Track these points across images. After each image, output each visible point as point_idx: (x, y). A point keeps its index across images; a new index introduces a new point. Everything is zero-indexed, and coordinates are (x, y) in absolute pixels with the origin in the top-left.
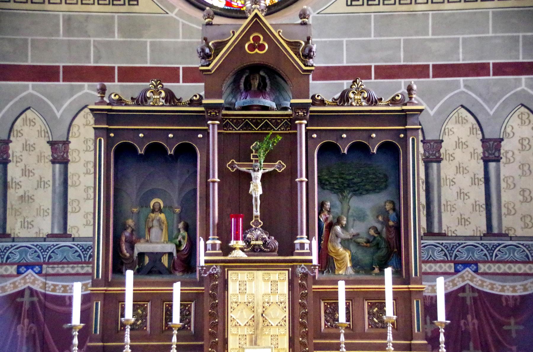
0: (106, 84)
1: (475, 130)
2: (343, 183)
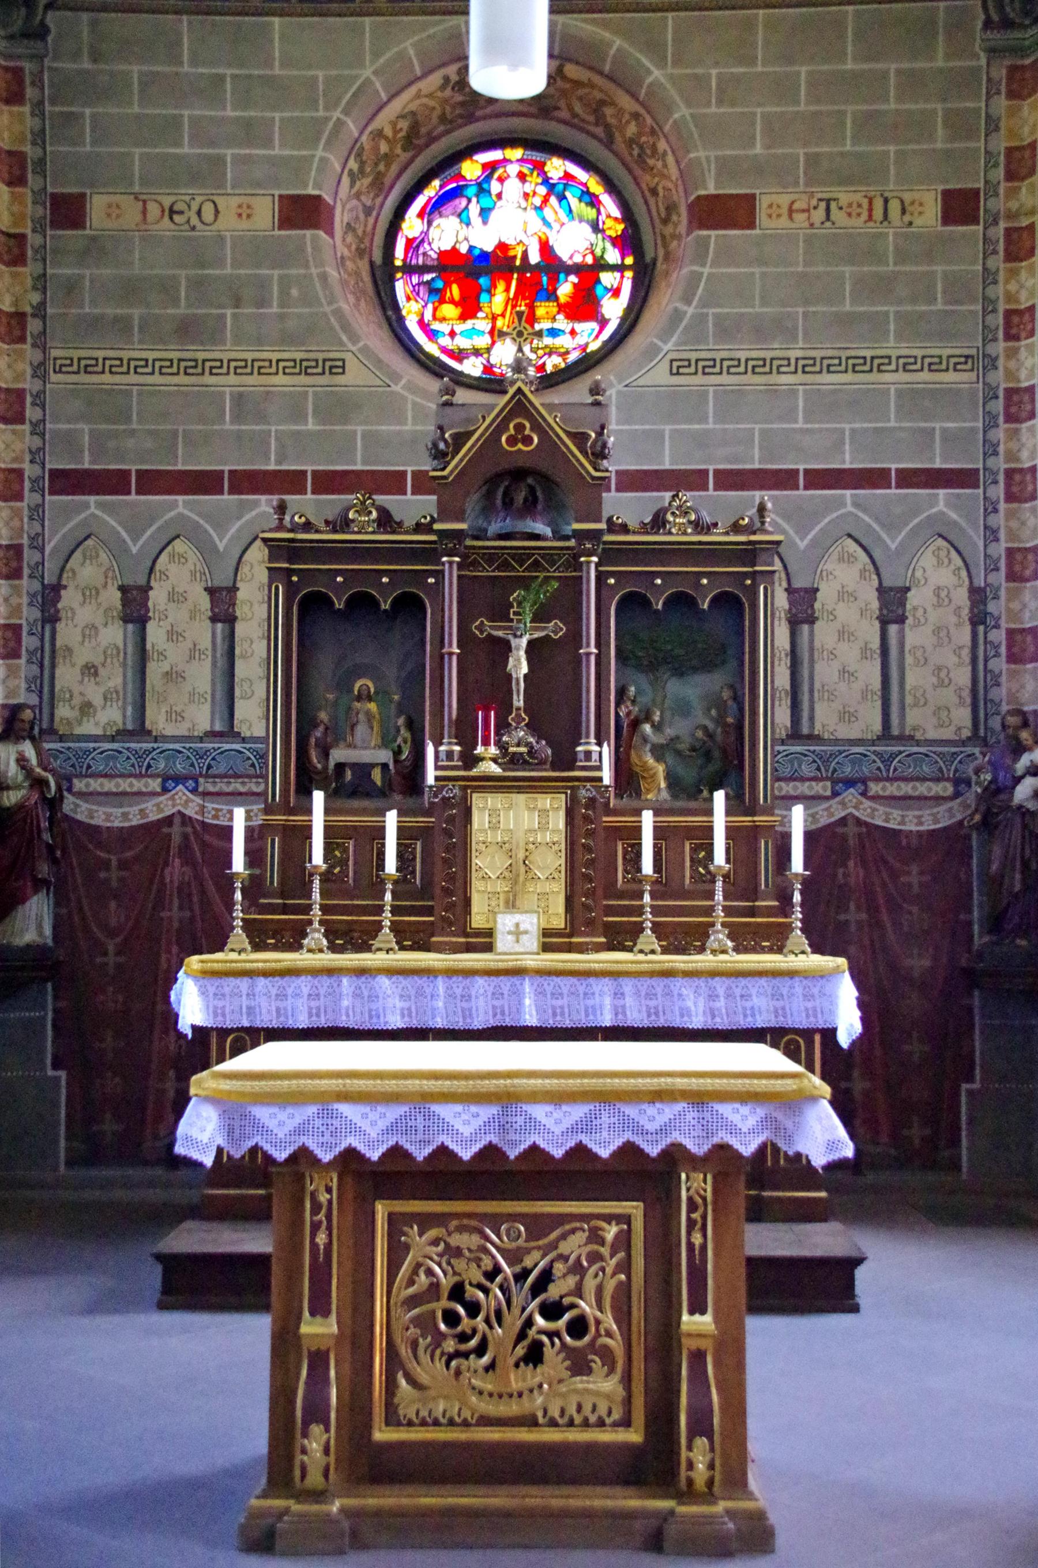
0: (286, 497)
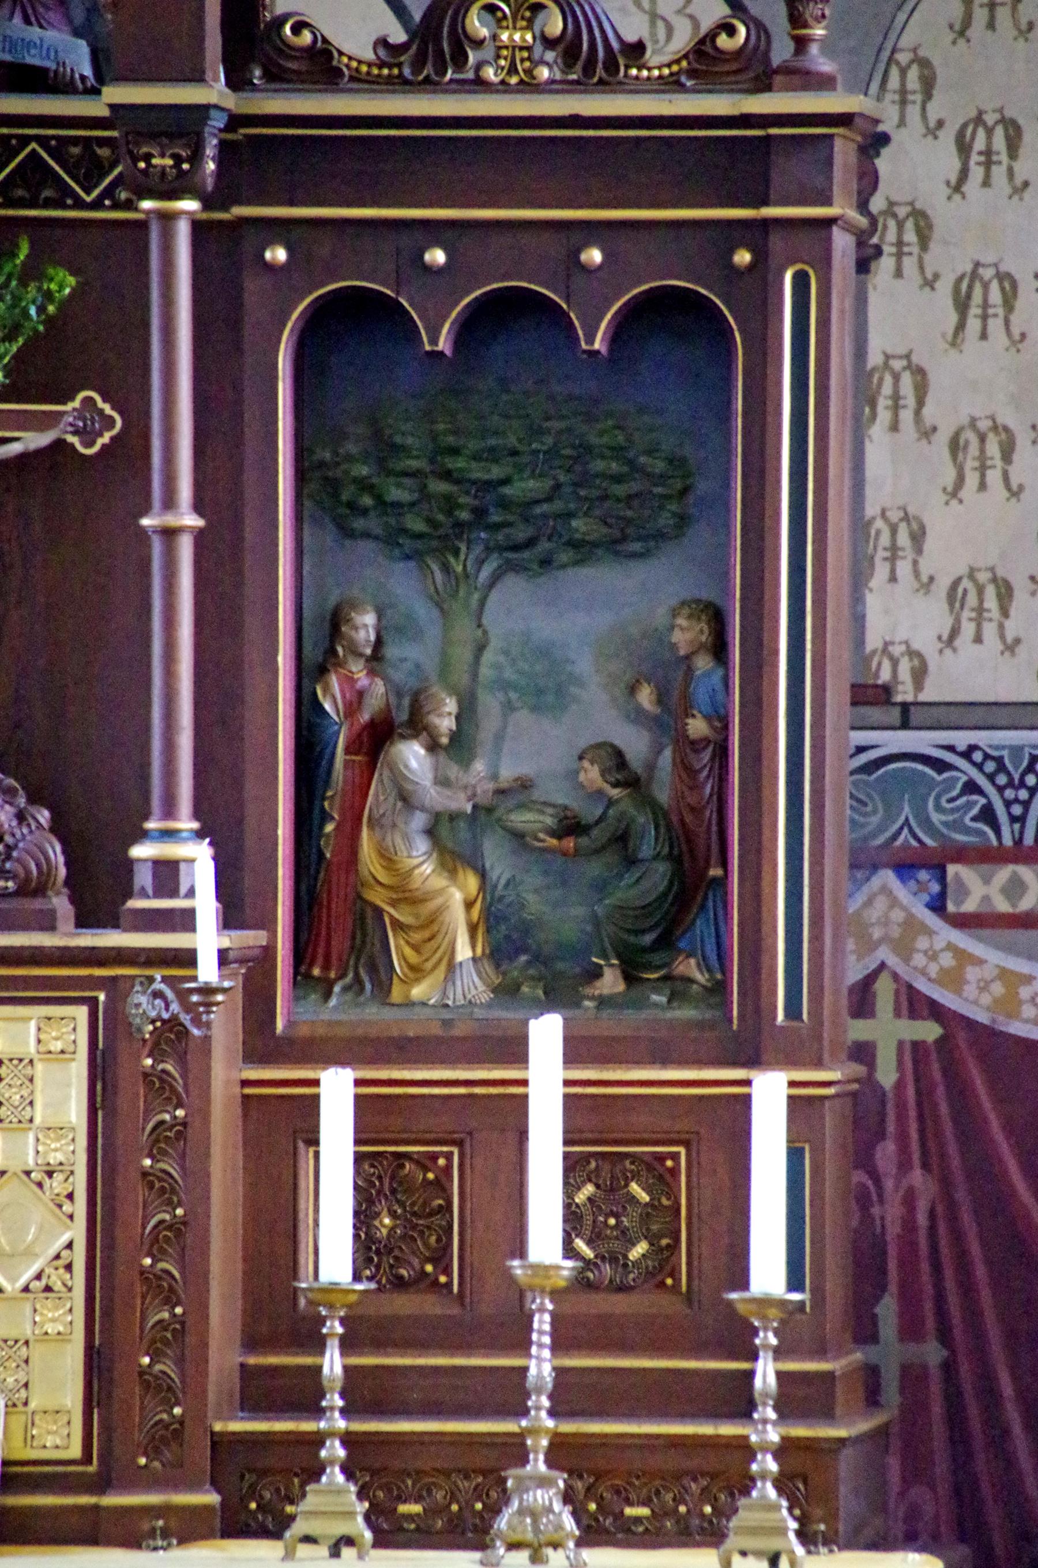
2: (450, 504)
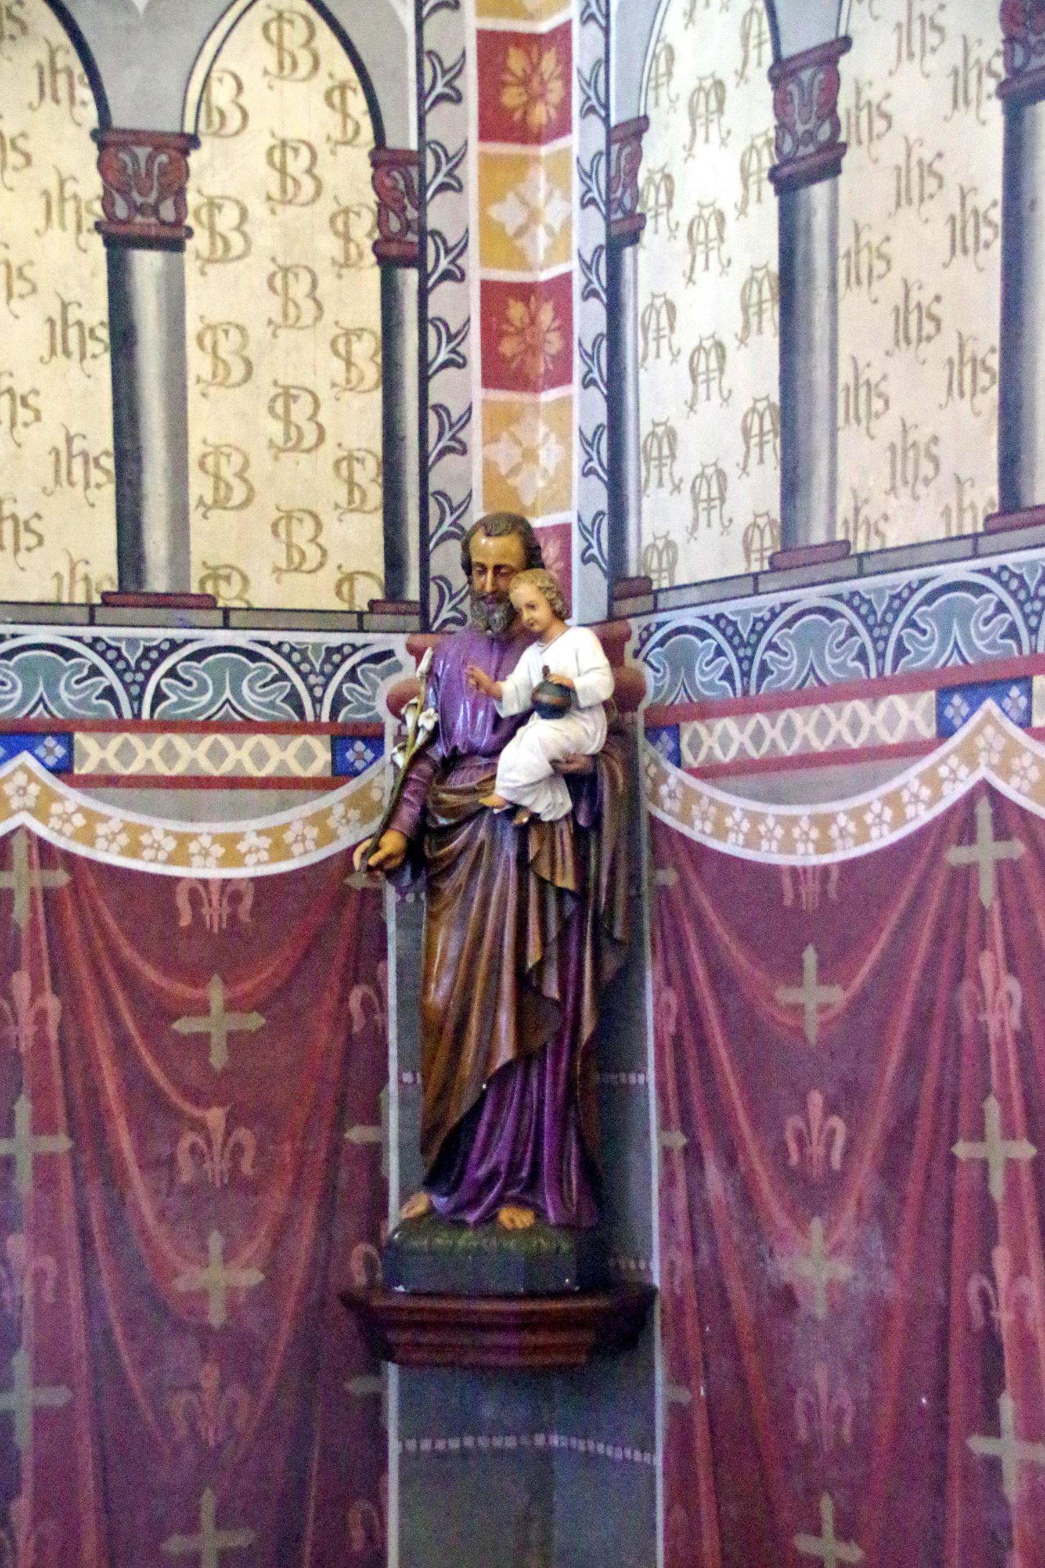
1: (62, 80)
